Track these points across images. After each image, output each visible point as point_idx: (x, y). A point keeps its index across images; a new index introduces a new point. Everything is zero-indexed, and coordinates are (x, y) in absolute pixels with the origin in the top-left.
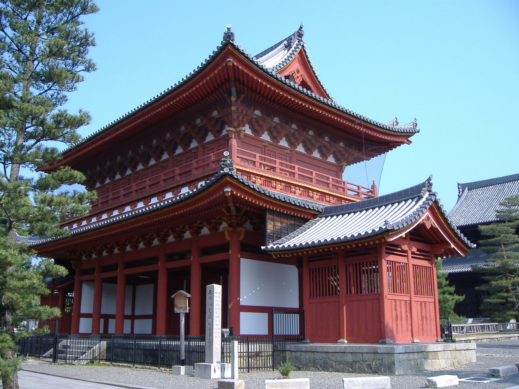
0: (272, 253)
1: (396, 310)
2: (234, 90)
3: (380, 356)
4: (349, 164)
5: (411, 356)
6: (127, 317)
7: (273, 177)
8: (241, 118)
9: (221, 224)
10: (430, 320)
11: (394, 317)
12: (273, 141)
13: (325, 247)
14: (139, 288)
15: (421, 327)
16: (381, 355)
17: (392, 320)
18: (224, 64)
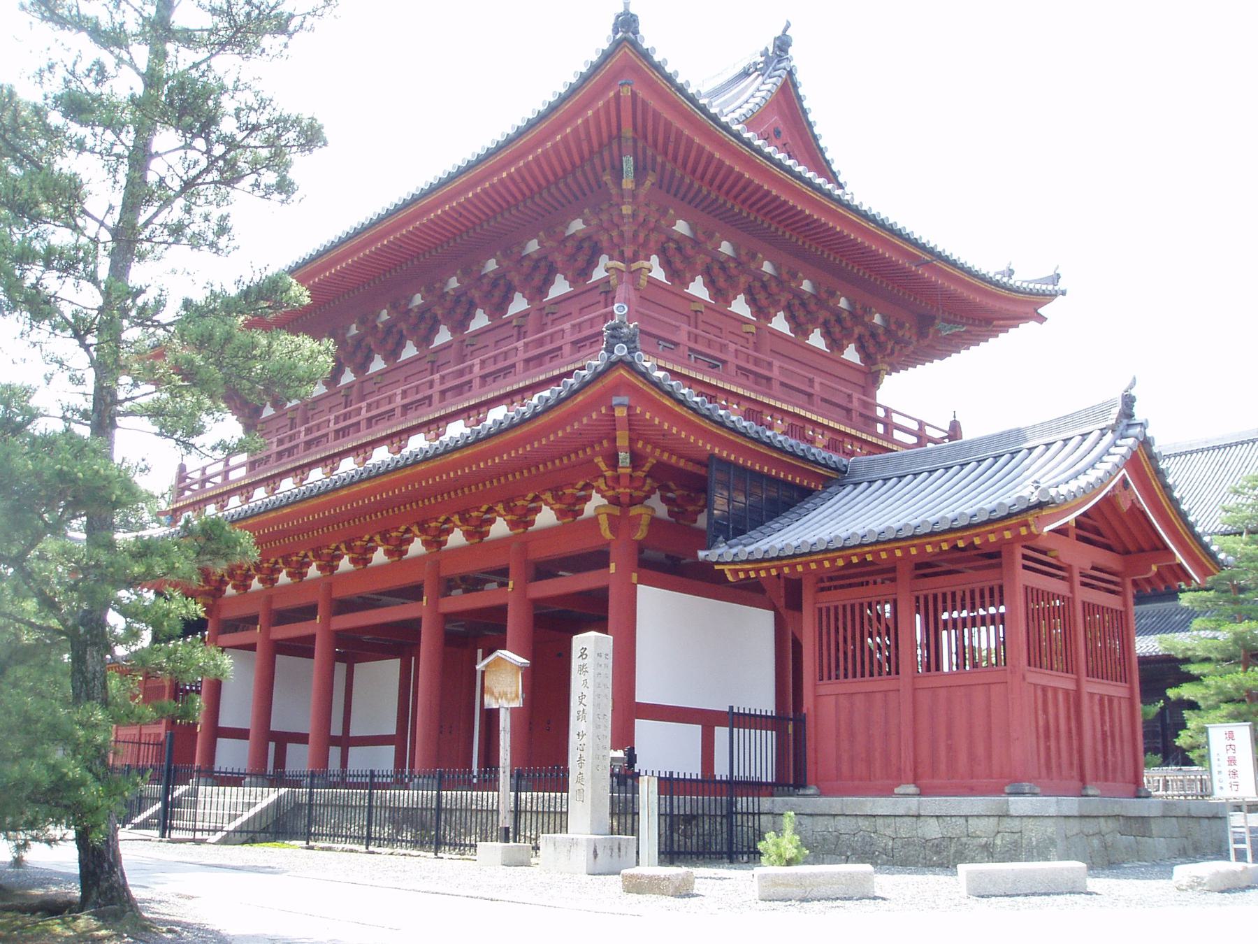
0: (726, 568)
1: (1045, 712)
2: (628, 163)
3: (1015, 824)
4: (894, 368)
5: (1090, 826)
6: (335, 741)
7: (720, 384)
8: (642, 235)
9: (587, 498)
10: (1122, 741)
11: (1041, 730)
12: (716, 300)
13: (867, 549)
14: (361, 669)
15: (1101, 759)
16: (1017, 822)
17: (1038, 738)
18: (612, 94)
